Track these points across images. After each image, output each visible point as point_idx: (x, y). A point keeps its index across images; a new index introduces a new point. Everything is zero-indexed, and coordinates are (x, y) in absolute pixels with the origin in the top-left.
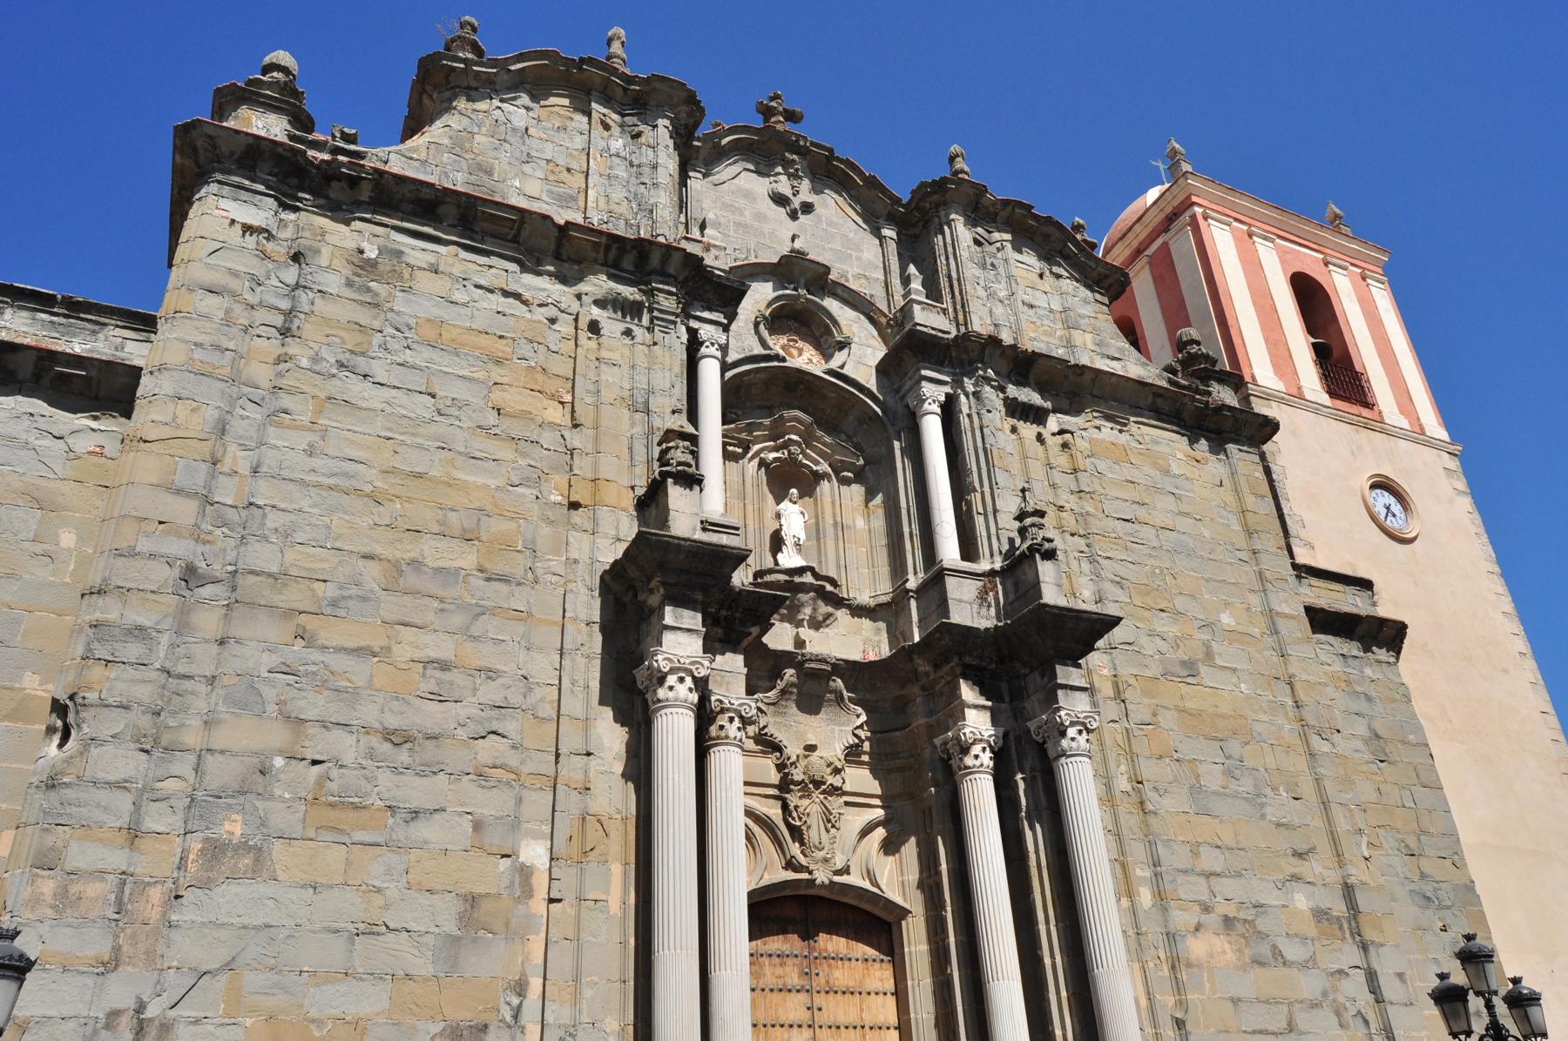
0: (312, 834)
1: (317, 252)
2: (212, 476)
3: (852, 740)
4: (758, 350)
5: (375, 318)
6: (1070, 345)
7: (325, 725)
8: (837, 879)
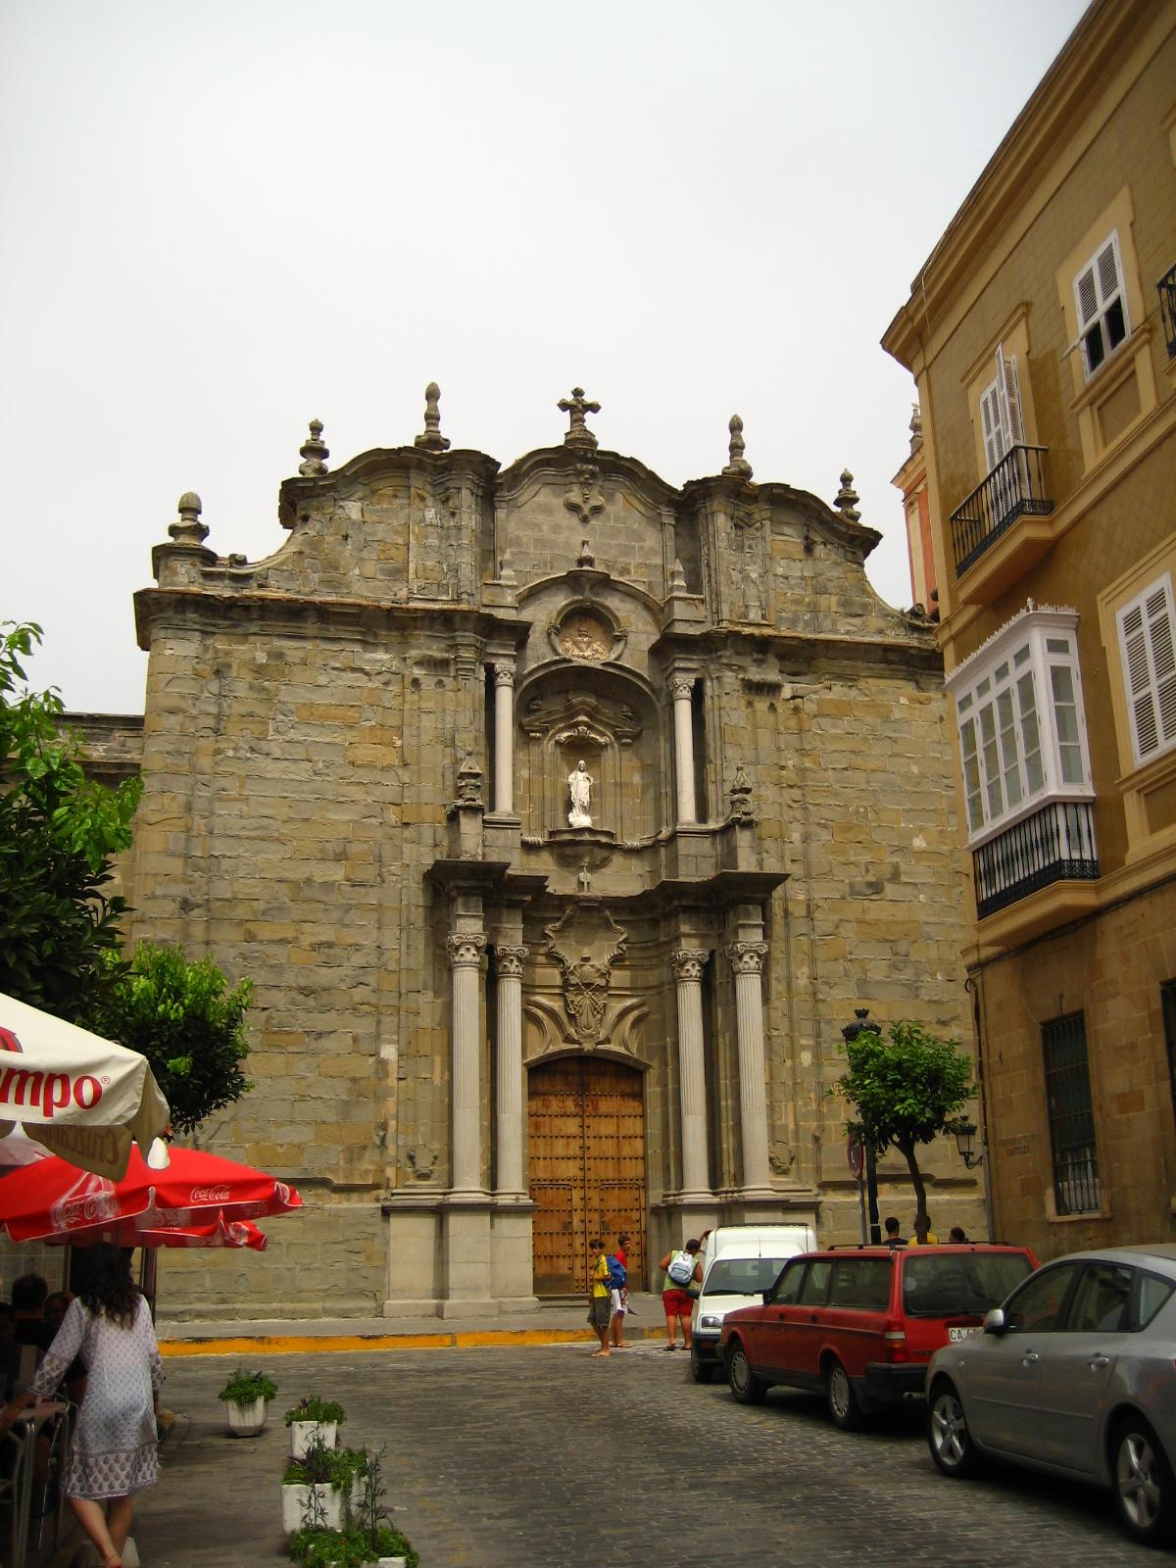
0: (266, 1049)
1: (230, 666)
2: (188, 839)
5: (270, 710)
7: (267, 987)
8: (599, 1047)
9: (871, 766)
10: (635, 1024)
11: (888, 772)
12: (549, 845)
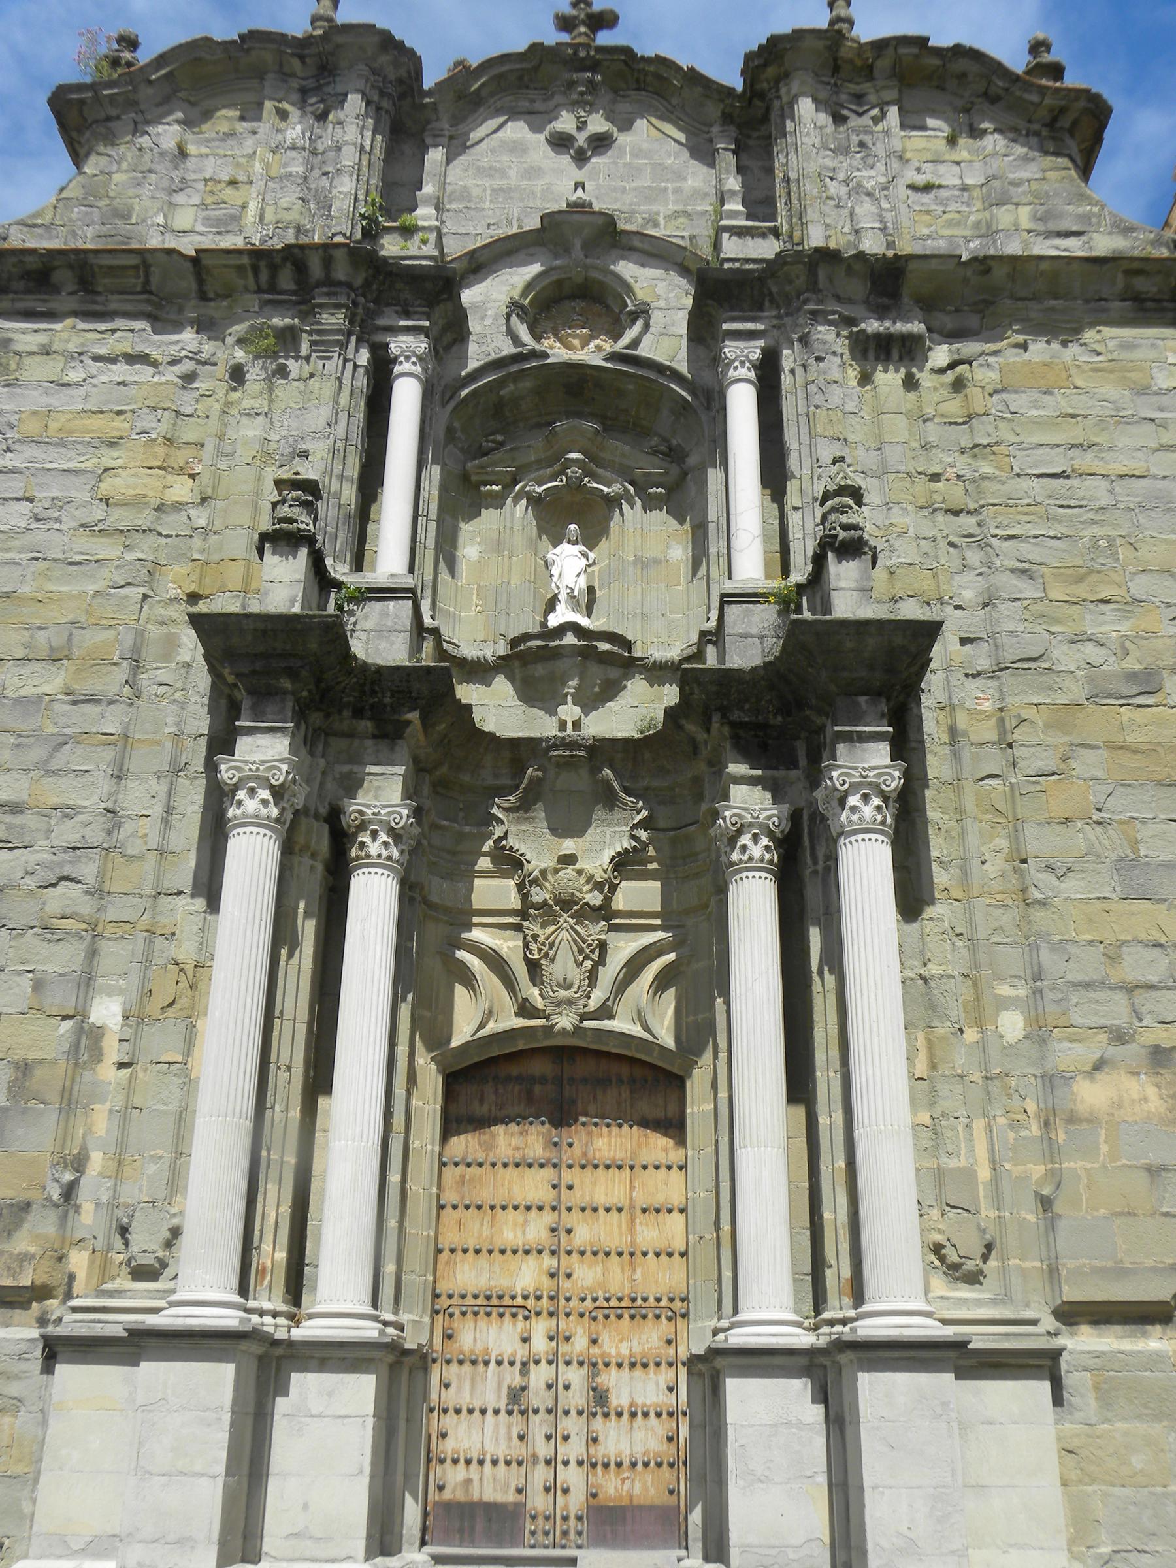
3: (627, 844)
4: (508, 349)
6: (988, 231)
8: (587, 1024)
9: (1117, 468)
10: (661, 983)
11: (1155, 477)
12: (503, 665)
